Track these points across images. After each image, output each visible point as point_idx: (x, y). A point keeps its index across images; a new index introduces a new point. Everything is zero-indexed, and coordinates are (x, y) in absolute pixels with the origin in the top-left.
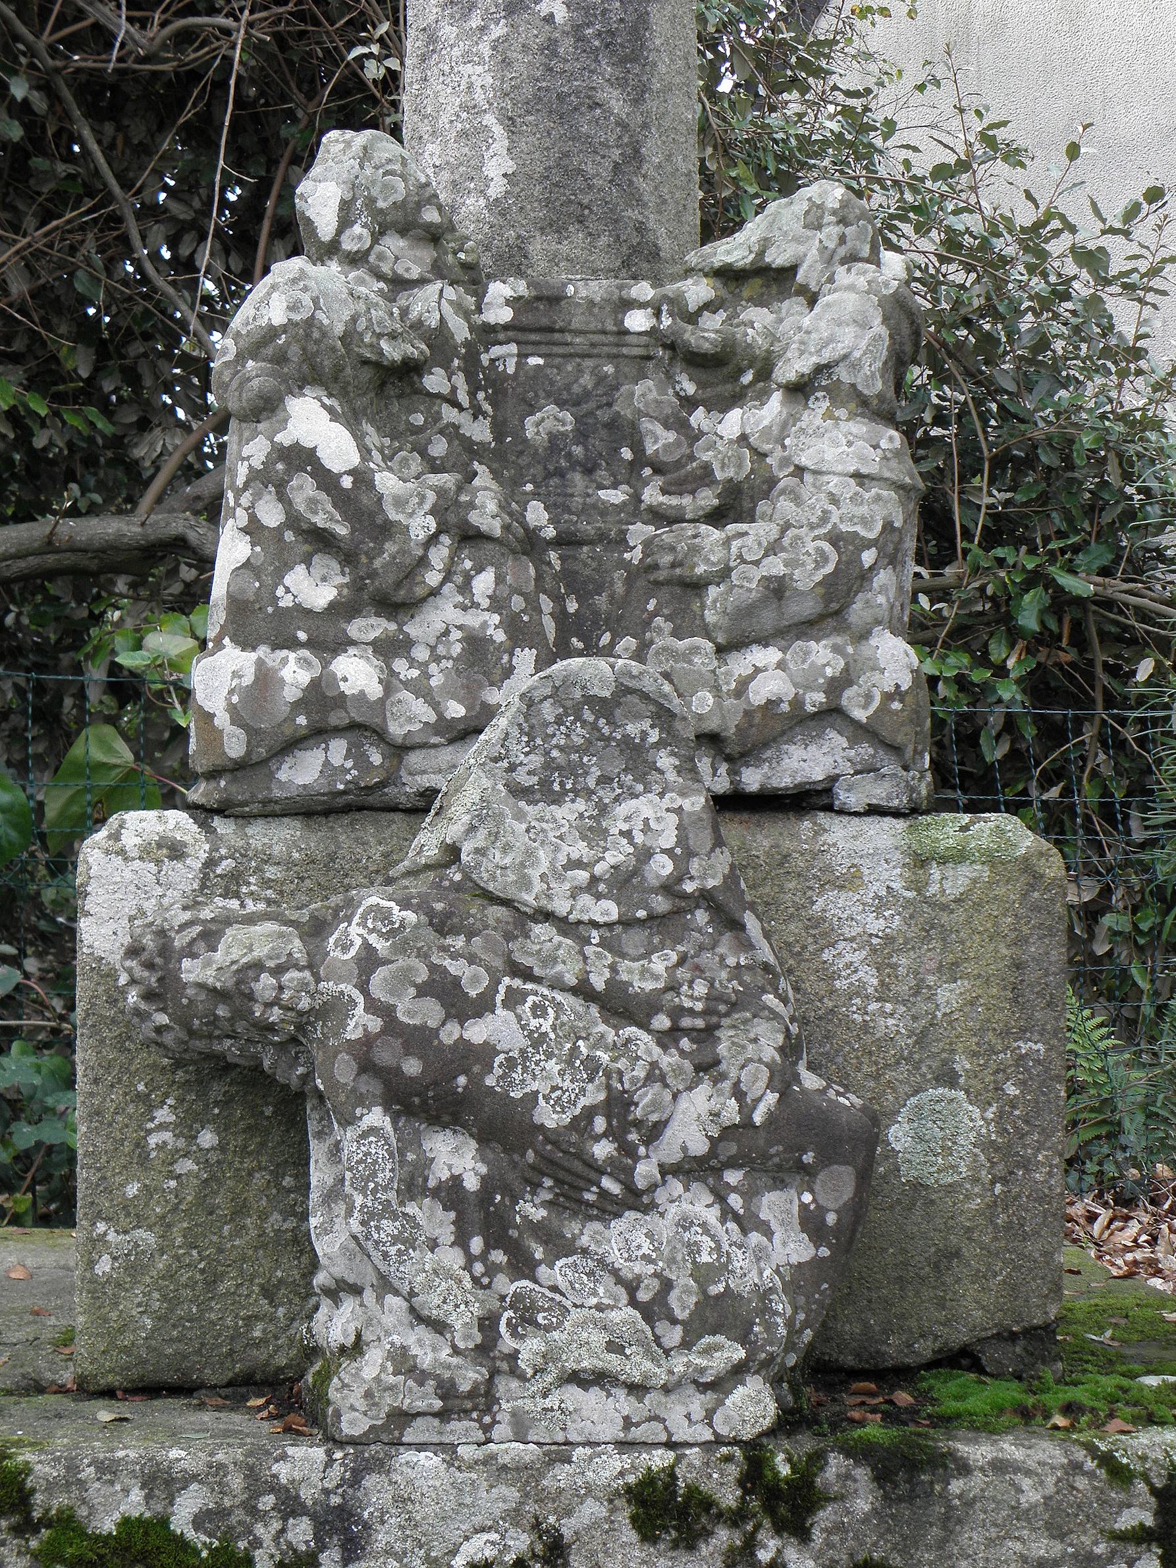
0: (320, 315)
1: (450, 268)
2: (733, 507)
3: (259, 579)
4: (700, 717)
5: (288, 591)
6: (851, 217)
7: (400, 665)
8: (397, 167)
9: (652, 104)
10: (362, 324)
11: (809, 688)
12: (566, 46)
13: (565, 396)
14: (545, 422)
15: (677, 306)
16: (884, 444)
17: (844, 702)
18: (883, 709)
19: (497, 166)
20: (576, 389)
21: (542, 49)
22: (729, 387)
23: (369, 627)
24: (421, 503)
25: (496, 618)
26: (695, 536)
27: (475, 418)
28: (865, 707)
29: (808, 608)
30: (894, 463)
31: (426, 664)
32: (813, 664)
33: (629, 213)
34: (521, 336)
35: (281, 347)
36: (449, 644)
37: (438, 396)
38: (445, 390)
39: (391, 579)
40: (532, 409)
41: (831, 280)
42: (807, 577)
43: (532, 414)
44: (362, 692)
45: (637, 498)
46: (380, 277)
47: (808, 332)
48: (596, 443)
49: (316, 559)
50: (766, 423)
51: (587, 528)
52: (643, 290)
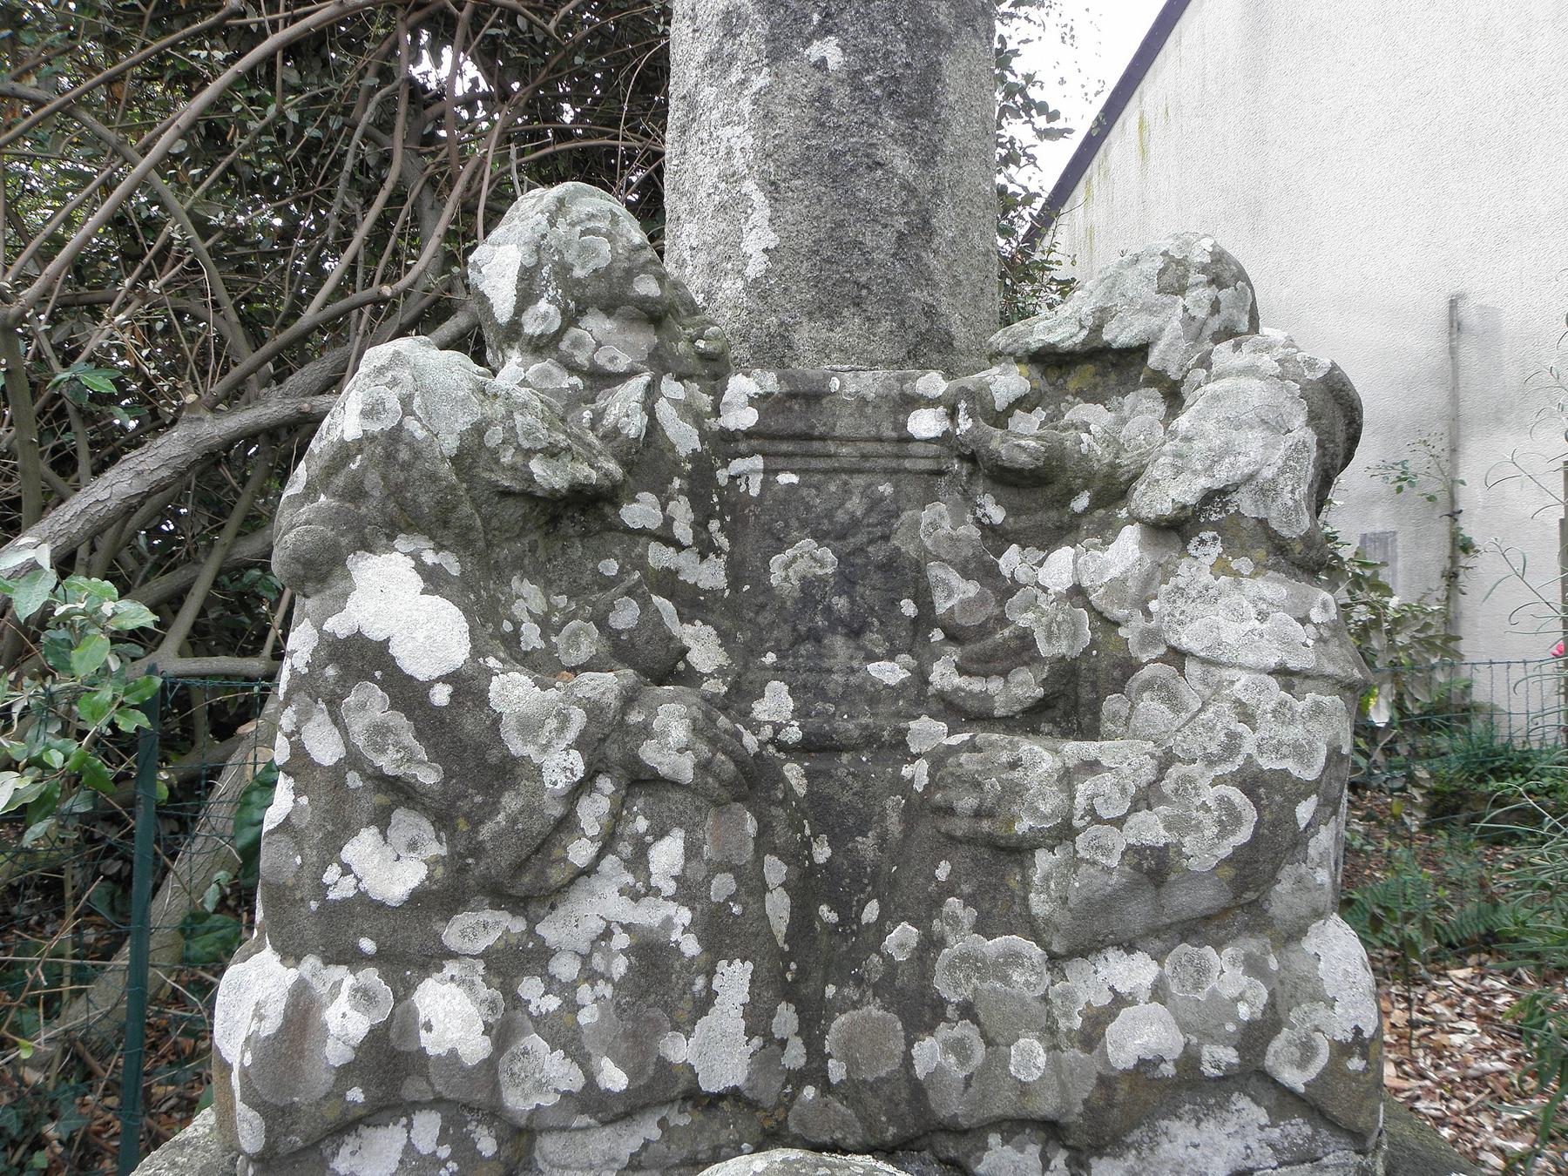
0: (412, 425)
1: (679, 359)
2: (1070, 703)
3: (301, 851)
4: (1024, 1089)
5: (346, 870)
6: (1227, 275)
7: (530, 988)
8: (604, 225)
9: (944, 169)
10: (494, 436)
11: (1208, 1036)
12: (841, 96)
13: (826, 525)
14: (799, 562)
15: (980, 404)
16: (1316, 615)
17: (1269, 1061)
18: (1334, 1069)
19: (758, 239)
20: (841, 516)
21: (812, 101)
22: (1053, 514)
23: (479, 929)
24: (561, 729)
25: (684, 916)
26: (1014, 765)
27: (703, 557)
28: (1302, 1064)
29: (1206, 898)
30: (1334, 648)
31: (573, 986)
32: (1214, 994)
33: (917, 294)
34: (768, 446)
35: (354, 475)
36: (609, 955)
37: (643, 532)
38: (654, 521)
39: (506, 858)
40: (781, 544)
41: (1205, 362)
42: (1206, 850)
43: (780, 551)
44: (453, 1053)
45: (921, 676)
46: (573, 369)
47: (1187, 439)
48: (867, 592)
49: (399, 815)
50: (1114, 572)
51: (848, 726)
52: (933, 383)
